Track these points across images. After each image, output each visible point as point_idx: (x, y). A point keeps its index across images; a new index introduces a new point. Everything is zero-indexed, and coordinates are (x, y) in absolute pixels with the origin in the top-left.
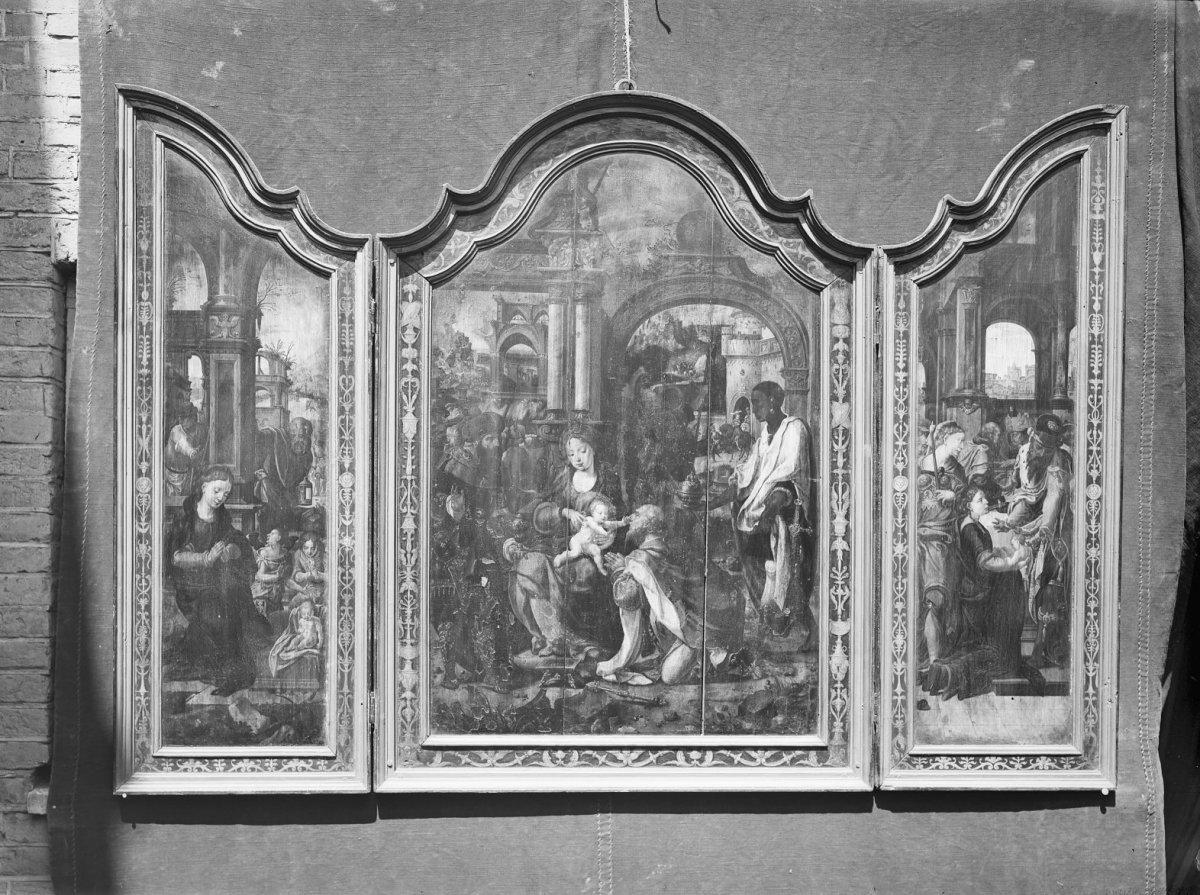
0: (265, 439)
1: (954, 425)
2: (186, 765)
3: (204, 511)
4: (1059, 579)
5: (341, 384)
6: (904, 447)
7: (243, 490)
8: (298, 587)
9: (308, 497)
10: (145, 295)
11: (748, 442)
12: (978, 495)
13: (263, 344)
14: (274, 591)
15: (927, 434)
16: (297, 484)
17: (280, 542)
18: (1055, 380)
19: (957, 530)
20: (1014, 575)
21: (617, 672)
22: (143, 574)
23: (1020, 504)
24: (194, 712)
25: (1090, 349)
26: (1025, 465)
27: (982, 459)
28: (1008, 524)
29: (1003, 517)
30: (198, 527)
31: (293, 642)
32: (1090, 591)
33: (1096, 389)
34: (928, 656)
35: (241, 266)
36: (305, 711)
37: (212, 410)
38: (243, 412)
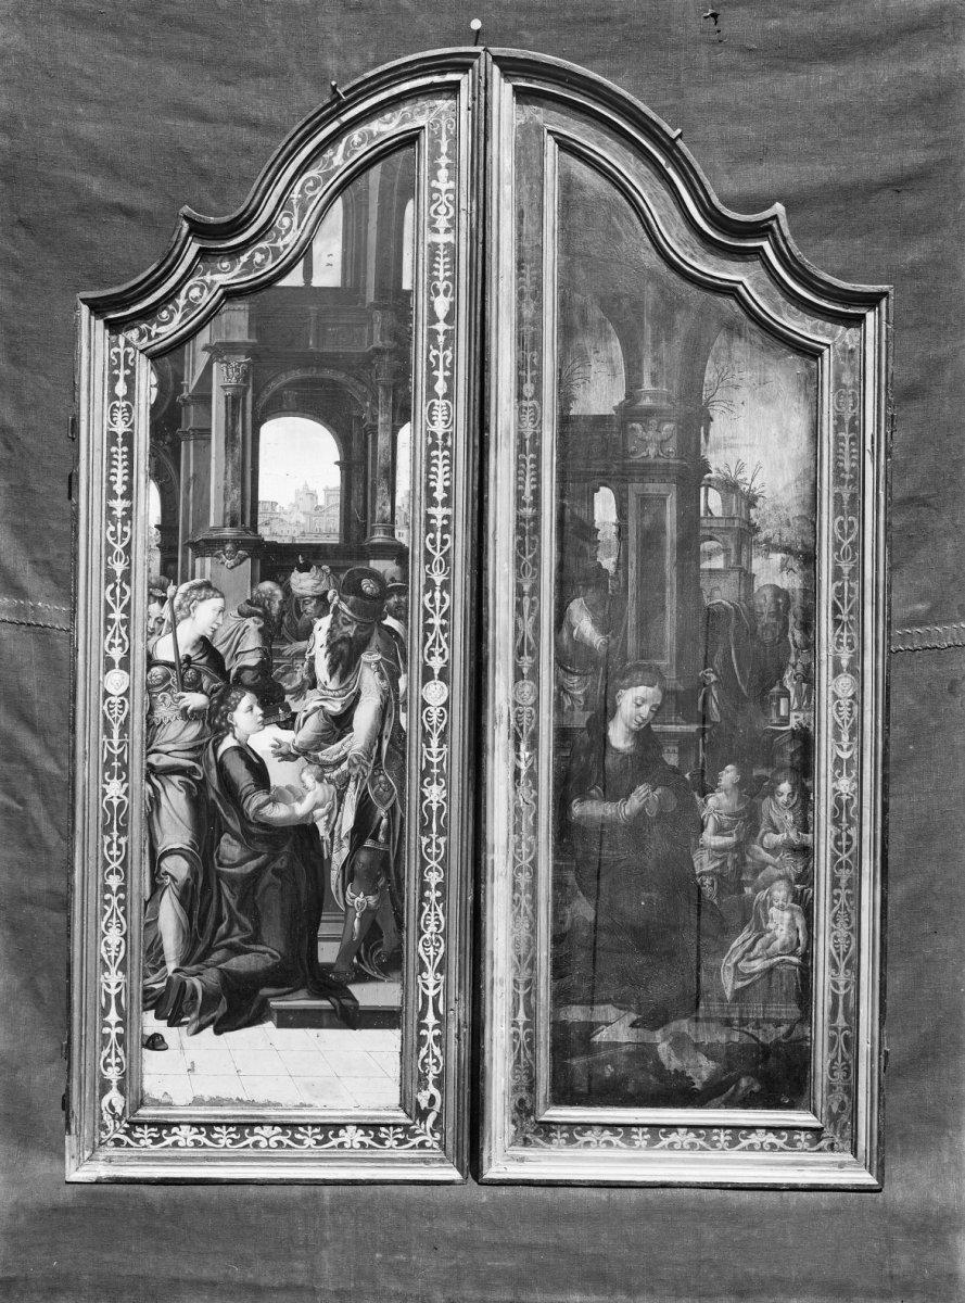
0: (711, 616)
1: (207, 585)
2: (590, 1136)
4: (381, 837)
5: (837, 531)
6: (124, 622)
7: (676, 702)
8: (768, 857)
9: (783, 713)
10: (529, 389)
12: (248, 699)
13: (713, 467)
14: (729, 864)
15: (162, 601)
16: (765, 691)
17: (739, 785)
18: (374, 512)
19: (212, 758)
20: (304, 832)
22: (434, 836)
23: (315, 716)
24: (603, 1055)
25: (429, 458)
26: (324, 650)
27: (252, 641)
28: (296, 749)
29: (287, 736)
30: (609, 761)
31: (759, 945)
32: (429, 855)
33: (439, 523)
34: (163, 963)
35: (678, 341)
36: (778, 1055)
37: (632, 573)
38: (681, 577)
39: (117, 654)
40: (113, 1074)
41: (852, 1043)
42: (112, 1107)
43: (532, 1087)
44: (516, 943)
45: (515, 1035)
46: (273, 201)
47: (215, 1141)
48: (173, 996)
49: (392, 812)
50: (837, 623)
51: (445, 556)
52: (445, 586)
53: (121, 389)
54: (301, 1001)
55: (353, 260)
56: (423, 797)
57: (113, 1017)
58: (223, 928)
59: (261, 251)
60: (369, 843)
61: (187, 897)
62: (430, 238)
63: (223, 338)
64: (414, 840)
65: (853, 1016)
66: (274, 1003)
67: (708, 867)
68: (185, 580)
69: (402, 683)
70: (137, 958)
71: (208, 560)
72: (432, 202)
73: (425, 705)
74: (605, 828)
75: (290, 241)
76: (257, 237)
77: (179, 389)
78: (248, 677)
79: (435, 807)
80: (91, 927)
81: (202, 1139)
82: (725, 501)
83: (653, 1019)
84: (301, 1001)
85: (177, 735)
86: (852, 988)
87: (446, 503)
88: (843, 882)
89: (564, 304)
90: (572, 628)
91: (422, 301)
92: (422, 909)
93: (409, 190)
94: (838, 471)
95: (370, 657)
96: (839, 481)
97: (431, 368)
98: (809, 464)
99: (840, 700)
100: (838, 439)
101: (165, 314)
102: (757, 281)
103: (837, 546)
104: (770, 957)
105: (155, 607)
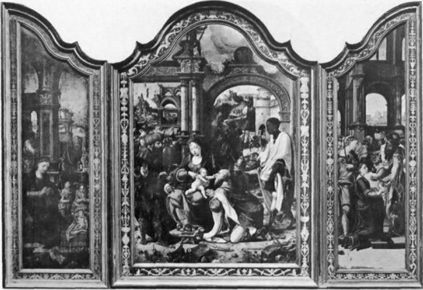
0: (62, 145)
2: (33, 276)
3: (38, 175)
4: (399, 200)
5: (94, 122)
7: (53, 166)
11: (264, 143)
12: (364, 166)
13: (62, 106)
15: (341, 141)
20: (379, 198)
21: (212, 238)
27: (365, 151)
29: (374, 175)
34: (343, 233)
39: (330, 155)
40: (330, 261)
41: (100, 252)
42: (331, 269)
43: (18, 264)
44: (13, 227)
45: (13, 251)
46: (368, 39)
47: (358, 278)
48: (346, 240)
49: (402, 194)
50: (95, 145)
51: (415, 129)
52: (415, 136)
53: (330, 87)
54: (379, 242)
55: (389, 53)
56: (410, 190)
57: (330, 246)
58: (359, 223)
59: (366, 51)
60: (396, 202)
61: (349, 216)
62: (409, 47)
63: (356, 74)
64: (408, 200)
65: (100, 245)
66: (372, 243)
67: (62, 207)
68: (347, 136)
69: (404, 161)
70: (336, 232)
71: (353, 131)
72: (409, 38)
73: (410, 167)
74: (35, 198)
75: (373, 48)
76: (364, 48)
77: (344, 87)
78: (364, 160)
79: (413, 192)
80: (325, 224)
81: (354, 277)
82: (65, 114)
83: (47, 247)
84: (379, 242)
85: (346, 176)
86: (100, 238)
87: (415, 115)
88: (97, 211)
89: (23, 64)
90: (26, 148)
91: (408, 63)
92: (410, 218)
93: (403, 36)
94: (94, 106)
95: (396, 155)
96: (94, 109)
97: (410, 81)
98: (86, 105)
99: (95, 165)
100: (94, 98)
101: (341, 68)
102: (72, 58)
103: (94, 126)
104: (79, 230)
105: (340, 143)
